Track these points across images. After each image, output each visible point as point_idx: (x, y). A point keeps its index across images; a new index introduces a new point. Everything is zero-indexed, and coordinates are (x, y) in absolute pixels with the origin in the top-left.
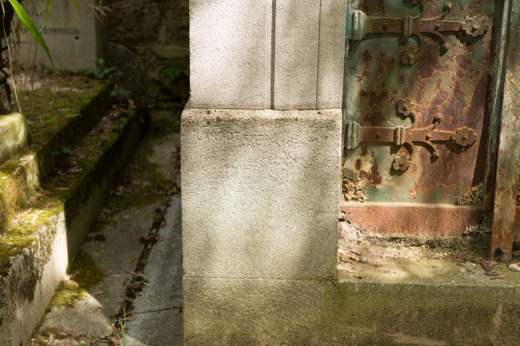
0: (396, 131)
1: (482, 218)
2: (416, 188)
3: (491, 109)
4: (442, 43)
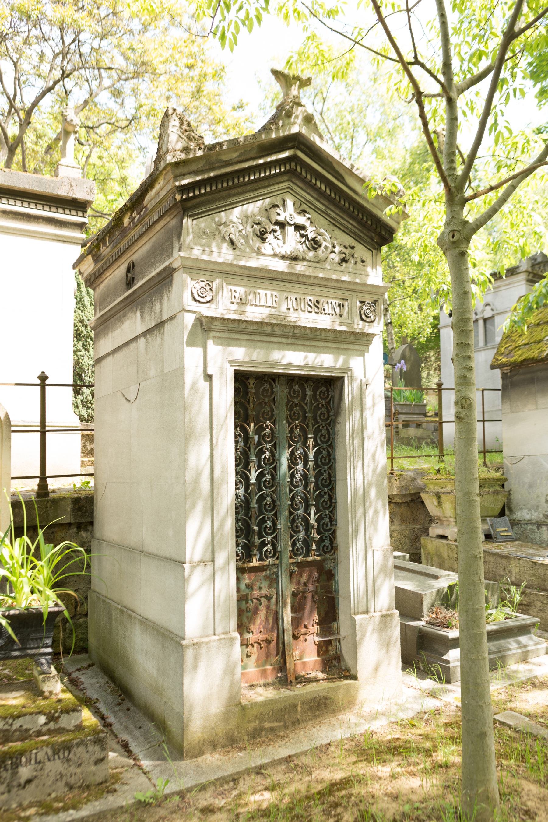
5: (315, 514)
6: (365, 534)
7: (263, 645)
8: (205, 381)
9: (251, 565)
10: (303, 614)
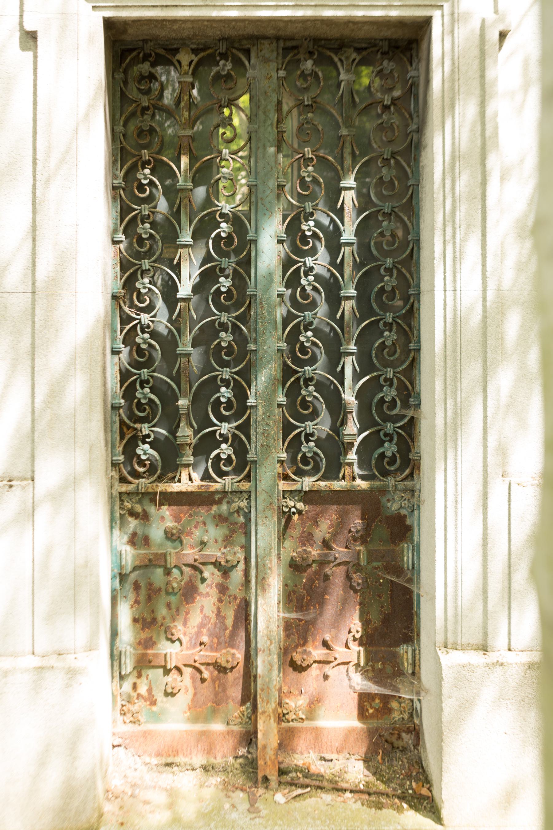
0: (166, 655)
1: (251, 740)
2: (190, 709)
4: (201, 572)
5: (357, 377)
6: (485, 439)
7: (206, 675)
8: (24, 48)
9: (175, 487)
10: (321, 614)
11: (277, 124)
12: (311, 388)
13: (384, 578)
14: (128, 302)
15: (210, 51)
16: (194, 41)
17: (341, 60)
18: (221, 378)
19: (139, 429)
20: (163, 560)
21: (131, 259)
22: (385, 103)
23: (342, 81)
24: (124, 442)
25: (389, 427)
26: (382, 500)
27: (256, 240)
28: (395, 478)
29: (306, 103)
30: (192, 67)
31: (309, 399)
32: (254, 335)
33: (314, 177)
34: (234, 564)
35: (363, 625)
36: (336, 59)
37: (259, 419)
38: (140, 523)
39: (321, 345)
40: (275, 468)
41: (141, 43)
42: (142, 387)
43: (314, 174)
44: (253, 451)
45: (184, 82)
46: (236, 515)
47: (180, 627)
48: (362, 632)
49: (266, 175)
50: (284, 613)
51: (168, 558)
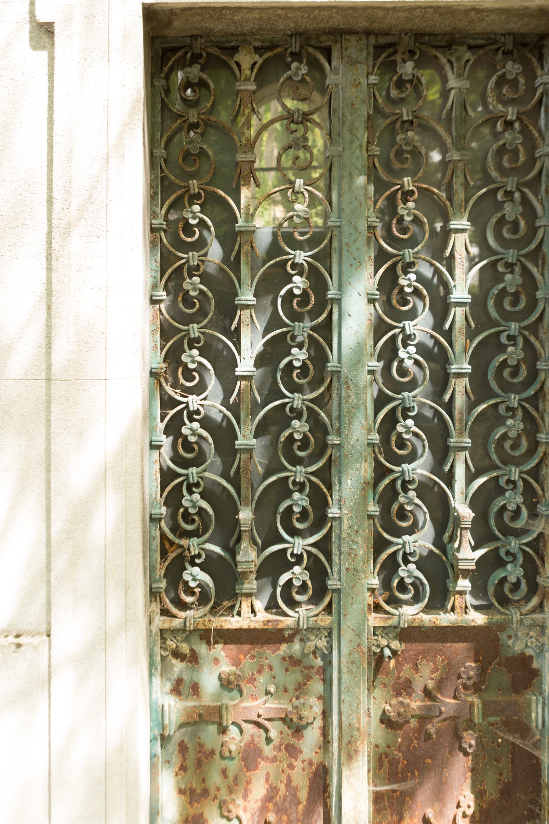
3: (331, 807)
8: (36, 45)
9: (233, 622)
11: (367, 146)
12: (412, 494)
13: (502, 738)
14: (170, 379)
15: (279, 50)
16: (258, 37)
17: (450, 62)
18: (294, 481)
19: (186, 547)
20: (217, 715)
21: (175, 324)
22: (509, 118)
23: (452, 88)
24: (167, 563)
25: (514, 544)
26: (500, 637)
27: (340, 299)
28: (518, 608)
29: (405, 118)
30: (255, 70)
31: (409, 508)
32: (337, 424)
33: (415, 216)
34: (310, 722)
35: (476, 798)
36: (444, 60)
37: (344, 535)
38: (187, 666)
39: (424, 437)
40: (364, 599)
41: (188, 40)
42: (191, 493)
43: (416, 212)
44: (336, 576)
45: (245, 91)
46: (311, 656)
47: (240, 801)
48: (476, 807)
49: (352, 213)
50: (375, 786)
51: (224, 713)
